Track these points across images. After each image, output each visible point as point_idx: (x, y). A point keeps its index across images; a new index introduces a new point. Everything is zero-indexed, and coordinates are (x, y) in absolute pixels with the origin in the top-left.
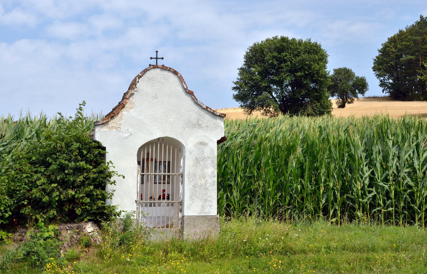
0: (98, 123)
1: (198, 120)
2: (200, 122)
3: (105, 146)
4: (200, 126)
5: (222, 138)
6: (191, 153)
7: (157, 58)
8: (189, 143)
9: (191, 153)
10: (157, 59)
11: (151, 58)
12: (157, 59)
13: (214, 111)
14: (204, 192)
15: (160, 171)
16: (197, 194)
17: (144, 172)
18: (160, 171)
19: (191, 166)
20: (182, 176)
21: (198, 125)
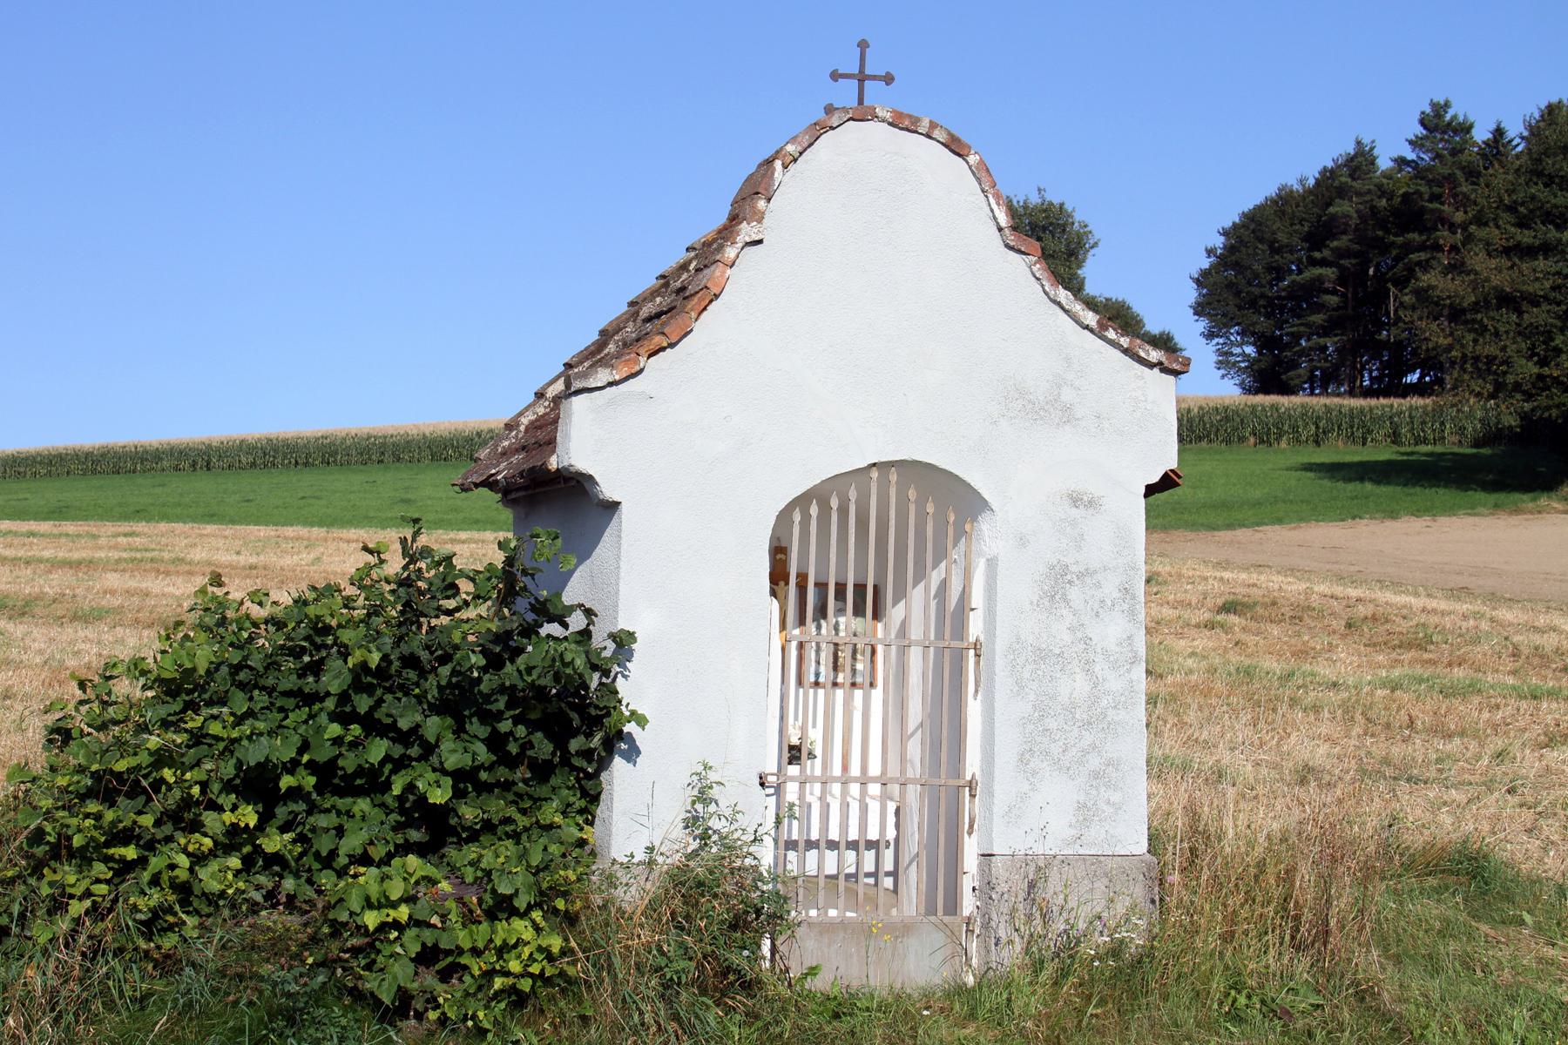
2: (1067, 395)
4: (1067, 416)
7: (862, 78)
14: (1088, 738)
16: (1056, 749)
20: (978, 656)
21: (1051, 409)
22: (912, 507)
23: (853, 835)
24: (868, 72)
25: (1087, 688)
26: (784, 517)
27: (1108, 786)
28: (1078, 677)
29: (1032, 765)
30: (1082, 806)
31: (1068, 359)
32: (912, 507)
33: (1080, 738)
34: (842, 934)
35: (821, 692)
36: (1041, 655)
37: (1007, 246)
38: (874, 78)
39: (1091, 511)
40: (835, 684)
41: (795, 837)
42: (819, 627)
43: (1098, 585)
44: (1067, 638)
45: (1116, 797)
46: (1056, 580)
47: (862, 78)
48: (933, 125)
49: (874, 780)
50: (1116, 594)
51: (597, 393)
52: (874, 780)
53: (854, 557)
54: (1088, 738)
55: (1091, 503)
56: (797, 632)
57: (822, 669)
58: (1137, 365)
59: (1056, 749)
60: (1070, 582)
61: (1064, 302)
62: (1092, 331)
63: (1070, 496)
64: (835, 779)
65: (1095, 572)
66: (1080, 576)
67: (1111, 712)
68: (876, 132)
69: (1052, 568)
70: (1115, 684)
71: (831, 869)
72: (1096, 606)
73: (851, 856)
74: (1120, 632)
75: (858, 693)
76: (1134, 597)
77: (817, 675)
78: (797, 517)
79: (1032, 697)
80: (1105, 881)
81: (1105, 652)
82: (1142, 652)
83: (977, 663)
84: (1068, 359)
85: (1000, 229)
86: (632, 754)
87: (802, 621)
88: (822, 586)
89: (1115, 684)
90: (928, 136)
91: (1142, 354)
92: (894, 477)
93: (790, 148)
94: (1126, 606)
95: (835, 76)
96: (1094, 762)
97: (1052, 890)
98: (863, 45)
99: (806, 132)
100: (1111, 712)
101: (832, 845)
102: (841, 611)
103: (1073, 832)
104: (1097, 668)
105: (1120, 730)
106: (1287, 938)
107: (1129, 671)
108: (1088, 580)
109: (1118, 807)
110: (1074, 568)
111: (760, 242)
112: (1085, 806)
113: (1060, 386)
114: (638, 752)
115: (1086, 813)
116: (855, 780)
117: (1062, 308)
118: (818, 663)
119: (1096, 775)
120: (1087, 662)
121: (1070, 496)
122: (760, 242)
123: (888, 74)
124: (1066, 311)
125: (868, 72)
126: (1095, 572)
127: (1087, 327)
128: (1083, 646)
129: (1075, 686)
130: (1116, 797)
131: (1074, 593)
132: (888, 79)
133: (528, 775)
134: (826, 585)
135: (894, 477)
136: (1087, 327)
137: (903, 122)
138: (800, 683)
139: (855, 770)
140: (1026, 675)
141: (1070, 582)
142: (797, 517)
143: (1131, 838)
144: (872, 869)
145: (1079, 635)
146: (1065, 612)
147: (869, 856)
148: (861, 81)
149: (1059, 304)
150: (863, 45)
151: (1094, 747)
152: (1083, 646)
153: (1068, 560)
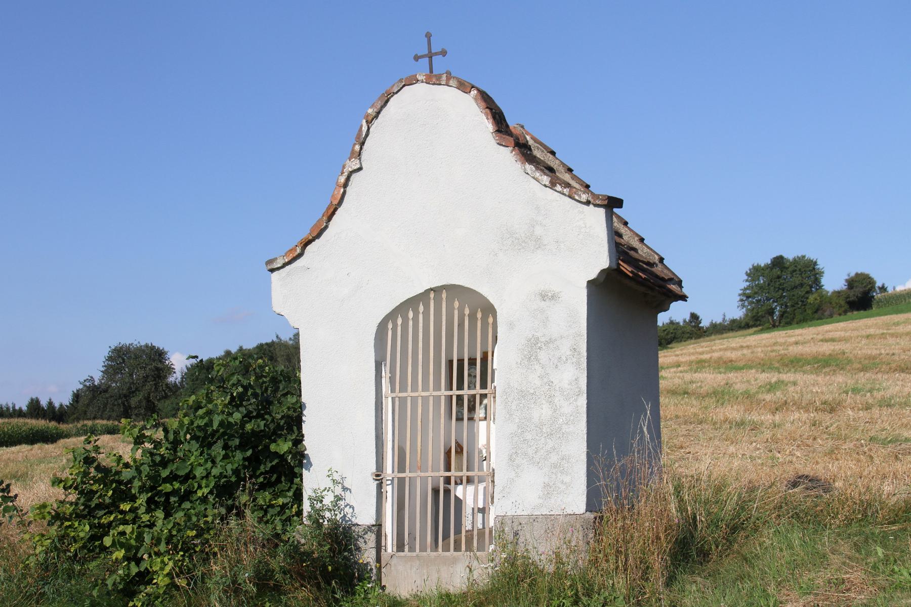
0: (276, 266)
2: (538, 231)
4: (539, 244)
9: (511, 326)
14: (550, 444)
16: (530, 451)
21: (527, 242)
22: (456, 312)
25: (550, 413)
28: (544, 406)
30: (546, 486)
32: (456, 312)
34: (418, 562)
38: (436, 54)
39: (553, 302)
43: (557, 348)
44: (538, 382)
47: (430, 56)
50: (569, 353)
54: (550, 444)
55: (554, 297)
59: (530, 451)
60: (540, 348)
63: (541, 294)
65: (556, 340)
66: (547, 343)
67: (564, 427)
68: (420, 89)
70: (567, 409)
72: (556, 361)
78: (390, 326)
81: (561, 390)
88: (461, 362)
91: (577, 198)
92: (444, 295)
93: (370, 111)
94: (574, 360)
96: (554, 458)
98: (428, 36)
99: (379, 99)
100: (564, 427)
103: (541, 501)
104: (556, 400)
106: (199, 583)
107: (576, 400)
108: (551, 345)
110: (543, 339)
115: (548, 490)
119: (555, 466)
121: (541, 294)
122: (360, 169)
125: (433, 51)
126: (556, 340)
128: (548, 387)
129: (542, 412)
130: (567, 479)
132: (444, 53)
134: (476, 359)
135: (444, 295)
136: (545, 186)
140: (514, 407)
141: (540, 348)
142: (390, 326)
143: (575, 500)
145: (545, 380)
146: (537, 367)
148: (431, 58)
150: (428, 36)
152: (548, 387)
153: (539, 334)
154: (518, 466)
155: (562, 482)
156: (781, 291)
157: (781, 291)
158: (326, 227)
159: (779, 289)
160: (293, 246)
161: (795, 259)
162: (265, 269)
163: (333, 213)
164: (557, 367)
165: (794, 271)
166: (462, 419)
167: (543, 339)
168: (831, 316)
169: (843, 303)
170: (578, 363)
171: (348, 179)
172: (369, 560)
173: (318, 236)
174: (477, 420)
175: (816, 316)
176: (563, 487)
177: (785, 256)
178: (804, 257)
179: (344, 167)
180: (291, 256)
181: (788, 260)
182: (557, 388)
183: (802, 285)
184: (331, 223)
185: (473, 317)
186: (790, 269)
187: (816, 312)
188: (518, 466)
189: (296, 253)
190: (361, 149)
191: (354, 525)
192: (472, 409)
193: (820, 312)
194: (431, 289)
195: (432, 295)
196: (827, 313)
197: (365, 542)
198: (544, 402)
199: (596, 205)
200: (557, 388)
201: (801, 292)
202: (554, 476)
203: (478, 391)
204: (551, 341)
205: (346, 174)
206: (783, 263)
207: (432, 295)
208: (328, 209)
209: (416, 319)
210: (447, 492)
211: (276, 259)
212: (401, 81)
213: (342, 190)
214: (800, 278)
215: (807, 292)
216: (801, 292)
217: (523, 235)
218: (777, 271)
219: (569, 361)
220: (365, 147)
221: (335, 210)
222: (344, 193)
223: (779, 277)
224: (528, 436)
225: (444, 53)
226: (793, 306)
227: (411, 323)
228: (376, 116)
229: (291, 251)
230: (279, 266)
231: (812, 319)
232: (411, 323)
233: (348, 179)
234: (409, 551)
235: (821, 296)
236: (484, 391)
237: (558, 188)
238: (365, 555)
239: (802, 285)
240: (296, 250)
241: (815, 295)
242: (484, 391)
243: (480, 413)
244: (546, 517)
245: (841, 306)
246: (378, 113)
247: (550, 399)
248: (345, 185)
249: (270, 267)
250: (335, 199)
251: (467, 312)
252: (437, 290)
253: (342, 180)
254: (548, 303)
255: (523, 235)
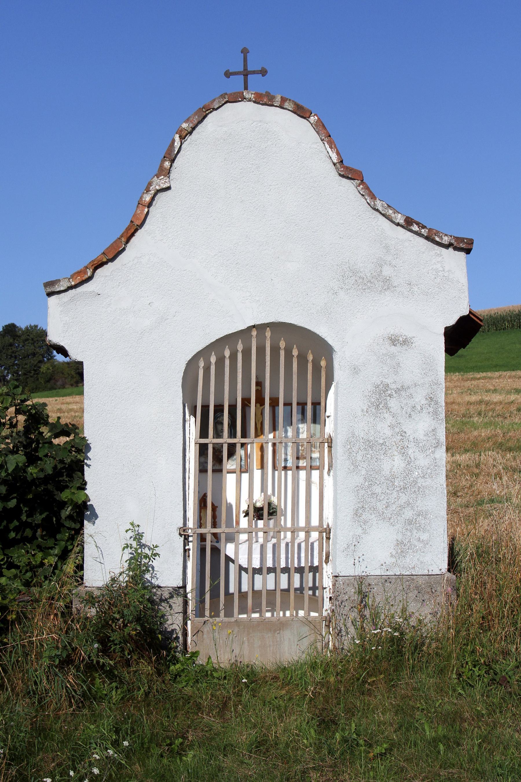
0: (57, 288)
1: (380, 264)
2: (387, 271)
3: (79, 359)
4: (387, 285)
5: (463, 320)
6: (355, 370)
7: (246, 74)
8: (353, 338)
9: (355, 370)
10: (245, 69)
11: (228, 74)
12: (245, 69)
13: (430, 230)
14: (404, 498)
15: (218, 434)
16: (380, 506)
17: (235, 437)
18: (218, 434)
19: (360, 413)
20: (330, 447)
21: (376, 282)
23: (256, 564)
24: (249, 69)
25: (403, 465)
26: (191, 365)
27: (418, 529)
28: (396, 458)
29: (364, 517)
30: (399, 543)
31: (387, 248)
33: (398, 498)
35: (290, 473)
36: (370, 444)
37: (340, 175)
38: (254, 72)
39: (405, 347)
40: (298, 467)
41: (303, 565)
42: (286, 432)
43: (411, 396)
44: (388, 432)
45: (424, 537)
46: (380, 394)
47: (246, 74)
48: (284, 100)
49: (315, 529)
50: (424, 402)
51: (63, 295)
52: (315, 529)
53: (256, 389)
55: (406, 342)
56: (271, 436)
57: (289, 458)
58: (436, 247)
59: (380, 506)
60: (390, 396)
61: (381, 210)
62: (402, 226)
64: (302, 529)
65: (409, 387)
66: (398, 391)
68: (246, 109)
69: (377, 386)
70: (423, 461)
71: (271, 586)
72: (409, 410)
73: (284, 578)
74: (428, 427)
75: (315, 474)
76: (437, 403)
77: (286, 460)
78: (202, 364)
79: (363, 472)
80: (416, 592)
81: (416, 441)
82: (443, 439)
83: (330, 451)
84: (387, 248)
85: (335, 164)
86: (94, 516)
87: (274, 428)
89: (423, 461)
90: (281, 107)
91: (437, 239)
92: (268, 334)
93: (185, 125)
94: (431, 410)
95: (228, 74)
96: (408, 514)
97: (377, 597)
98: (245, 52)
99: (196, 114)
100: (420, 480)
101: (270, 570)
102: (289, 421)
103: (393, 560)
104: (410, 452)
105: (427, 491)
107: (433, 452)
108: (403, 393)
109: (426, 543)
110: (393, 386)
111: (169, 188)
112: (402, 542)
113: (381, 266)
114: (96, 517)
115: (402, 548)
116: (302, 529)
117: (380, 213)
118: (286, 454)
119: (410, 522)
120: (403, 448)
122: (169, 188)
123: (263, 68)
124: (384, 215)
125: (249, 69)
126: (409, 387)
127: (398, 224)
128: (399, 437)
130: (424, 537)
131: (393, 403)
132: (263, 72)
133: (44, 533)
135: (268, 334)
137: (264, 99)
138: (274, 468)
139: (302, 523)
140: (359, 458)
141: (390, 396)
142: (202, 364)
143: (435, 561)
144: (286, 587)
145: (397, 430)
146: (386, 416)
147: (284, 578)
149: (377, 210)
150: (245, 52)
151: (408, 504)
152: (399, 437)
153: (388, 381)
154: (365, 522)
155: (419, 540)
156: (13, 359)
157: (13, 359)
158: (124, 249)
159: (11, 356)
160: (81, 267)
161: (27, 328)
162: (43, 292)
163: (133, 235)
164: (410, 416)
165: (27, 340)
166: (206, 471)
167: (393, 386)
168: (63, 387)
169: (73, 373)
170: (435, 413)
171: (153, 199)
172: (174, 627)
173: (112, 260)
174: (224, 471)
175: (49, 385)
176: (420, 545)
177: (18, 325)
178: (36, 326)
179: (150, 184)
180: (79, 279)
181: (20, 329)
182: (411, 439)
183: (34, 354)
184: (128, 245)
185: (302, 359)
186: (23, 338)
187: (48, 381)
188: (365, 522)
189: (86, 277)
190: (171, 166)
191: (154, 587)
192: (218, 459)
193: (52, 381)
194: (254, 326)
195: (254, 333)
196: (59, 383)
197: (170, 606)
198: (396, 453)
199: (456, 249)
200: (411, 439)
201: (33, 361)
202: (409, 534)
203: (226, 439)
204: (403, 388)
205: (153, 192)
206: (15, 331)
207: (254, 333)
208: (128, 229)
209: (233, 357)
210: (216, 551)
211: (59, 281)
212: (223, 96)
213: (146, 210)
214: (32, 347)
215: (40, 362)
216: (33, 361)
217: (369, 275)
218: (9, 339)
219: (425, 411)
220: (175, 164)
221: (136, 231)
222: (148, 213)
223: (11, 345)
224: (378, 490)
225: (263, 72)
226: (25, 374)
227: (227, 362)
228: (190, 133)
229: (79, 273)
230: (62, 289)
231: (44, 390)
232: (227, 362)
233: (153, 199)
234: (225, 616)
235: (54, 366)
236: (244, 441)
237: (415, 228)
238: (169, 622)
239: (34, 354)
240: (86, 273)
241: (47, 365)
242: (244, 441)
243: (230, 465)
244: (400, 577)
245: (72, 377)
246: (194, 129)
247: (403, 451)
248: (150, 205)
249: (49, 290)
250: (138, 219)
251: (295, 352)
252: (261, 328)
253: (147, 198)
254: (398, 348)
255: (369, 275)
